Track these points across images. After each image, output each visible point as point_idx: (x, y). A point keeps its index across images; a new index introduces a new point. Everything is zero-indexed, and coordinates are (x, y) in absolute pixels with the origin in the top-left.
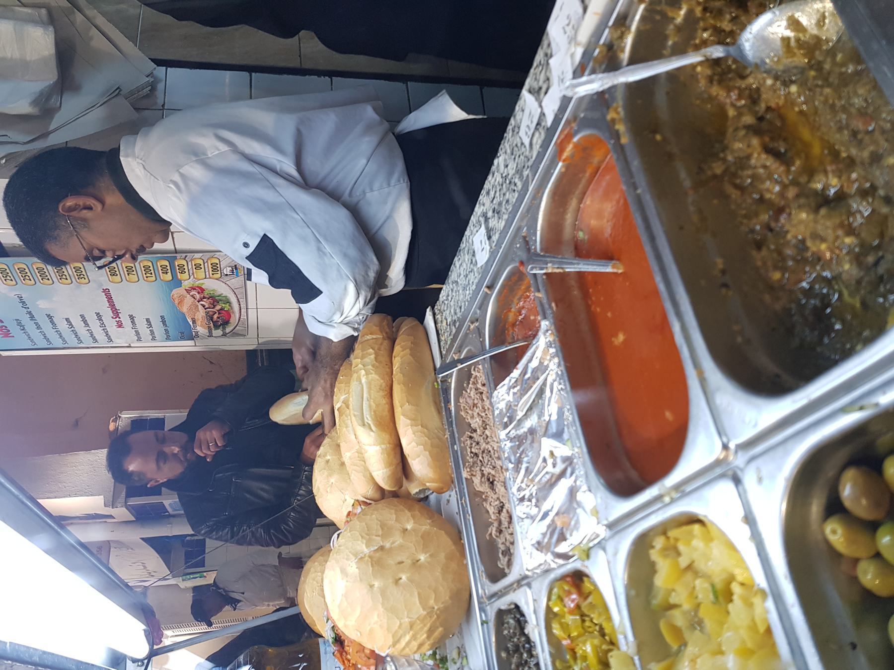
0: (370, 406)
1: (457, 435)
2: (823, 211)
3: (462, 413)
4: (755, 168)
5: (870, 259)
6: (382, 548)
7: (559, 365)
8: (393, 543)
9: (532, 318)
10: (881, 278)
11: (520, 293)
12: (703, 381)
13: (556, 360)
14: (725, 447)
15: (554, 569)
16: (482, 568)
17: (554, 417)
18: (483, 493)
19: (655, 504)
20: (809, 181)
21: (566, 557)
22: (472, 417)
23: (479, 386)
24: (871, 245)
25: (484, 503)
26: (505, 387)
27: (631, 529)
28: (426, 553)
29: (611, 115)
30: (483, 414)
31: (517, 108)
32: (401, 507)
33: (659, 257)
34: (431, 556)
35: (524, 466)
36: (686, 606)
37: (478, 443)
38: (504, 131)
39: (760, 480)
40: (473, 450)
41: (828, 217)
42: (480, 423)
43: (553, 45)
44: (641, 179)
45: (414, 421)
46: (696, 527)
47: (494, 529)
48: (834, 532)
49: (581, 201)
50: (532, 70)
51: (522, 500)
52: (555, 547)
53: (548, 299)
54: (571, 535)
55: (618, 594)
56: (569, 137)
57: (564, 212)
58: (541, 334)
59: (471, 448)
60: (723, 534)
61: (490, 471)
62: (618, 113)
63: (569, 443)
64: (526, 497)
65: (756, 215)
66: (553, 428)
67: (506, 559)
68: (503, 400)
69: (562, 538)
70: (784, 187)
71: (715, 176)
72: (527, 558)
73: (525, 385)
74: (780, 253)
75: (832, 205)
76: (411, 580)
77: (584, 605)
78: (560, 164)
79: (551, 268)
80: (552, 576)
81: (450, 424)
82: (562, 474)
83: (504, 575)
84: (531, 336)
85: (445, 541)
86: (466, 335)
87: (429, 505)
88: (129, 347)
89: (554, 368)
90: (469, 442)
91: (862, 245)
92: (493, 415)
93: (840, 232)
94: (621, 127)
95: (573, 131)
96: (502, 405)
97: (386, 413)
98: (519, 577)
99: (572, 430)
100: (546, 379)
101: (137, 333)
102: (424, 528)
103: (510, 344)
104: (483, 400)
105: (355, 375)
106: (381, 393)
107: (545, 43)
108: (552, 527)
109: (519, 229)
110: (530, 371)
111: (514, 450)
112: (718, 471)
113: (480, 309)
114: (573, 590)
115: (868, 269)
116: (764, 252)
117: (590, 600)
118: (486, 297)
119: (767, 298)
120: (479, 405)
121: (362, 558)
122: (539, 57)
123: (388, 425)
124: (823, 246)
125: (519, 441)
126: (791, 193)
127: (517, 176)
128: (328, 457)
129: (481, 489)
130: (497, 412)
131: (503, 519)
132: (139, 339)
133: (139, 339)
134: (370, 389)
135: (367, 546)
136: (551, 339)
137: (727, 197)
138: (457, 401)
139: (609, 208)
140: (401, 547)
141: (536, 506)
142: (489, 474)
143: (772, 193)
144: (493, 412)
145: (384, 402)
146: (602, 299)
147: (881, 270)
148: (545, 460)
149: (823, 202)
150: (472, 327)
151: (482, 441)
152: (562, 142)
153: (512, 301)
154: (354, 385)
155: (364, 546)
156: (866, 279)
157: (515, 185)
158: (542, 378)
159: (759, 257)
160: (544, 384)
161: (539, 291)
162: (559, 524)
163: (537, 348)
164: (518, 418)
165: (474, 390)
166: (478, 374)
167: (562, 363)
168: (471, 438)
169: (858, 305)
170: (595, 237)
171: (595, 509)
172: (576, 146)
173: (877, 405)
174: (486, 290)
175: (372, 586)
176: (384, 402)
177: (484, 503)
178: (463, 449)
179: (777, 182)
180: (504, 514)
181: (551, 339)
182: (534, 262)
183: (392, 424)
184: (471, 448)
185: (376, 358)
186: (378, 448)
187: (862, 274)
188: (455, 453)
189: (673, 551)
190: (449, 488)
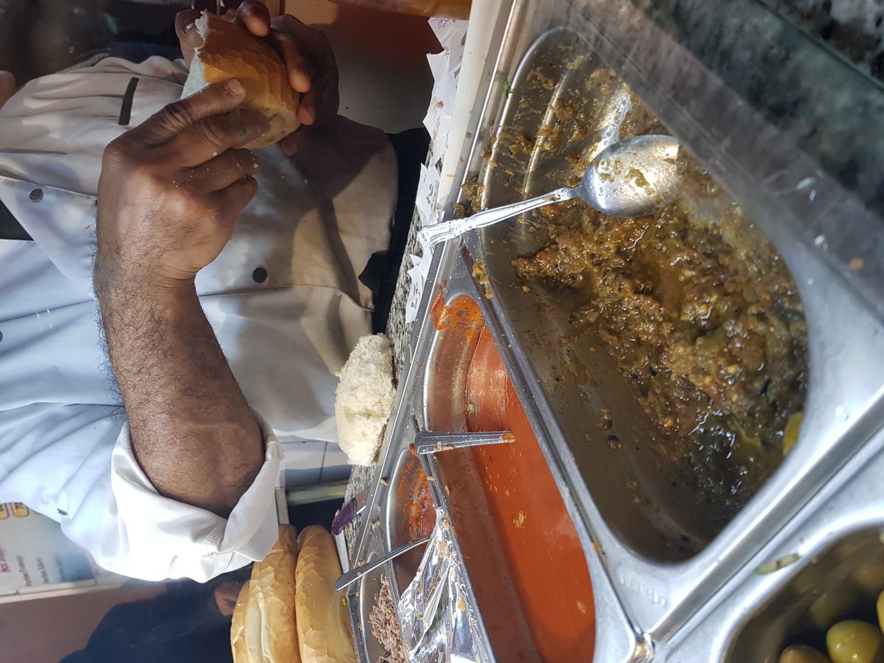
0: (269, 637)
2: (700, 341)
3: (374, 633)
4: (627, 312)
5: (758, 385)
10: (774, 405)
11: (420, 482)
12: (602, 555)
13: (454, 554)
14: (640, 640)
20: (680, 316)
24: (757, 371)
29: (476, 271)
30: (397, 632)
31: (397, 285)
33: (538, 414)
38: (389, 311)
41: (705, 347)
42: (395, 643)
49: (467, 370)
50: (407, 246)
53: (440, 482)
56: (442, 301)
62: (480, 268)
71: (589, 324)
74: (667, 397)
78: (437, 332)
79: (440, 447)
86: (370, 537)
88: (17, 594)
93: (721, 361)
96: (408, 618)
97: (288, 643)
101: (26, 576)
103: (414, 542)
105: (252, 600)
107: (415, 217)
115: (757, 397)
116: (651, 398)
118: (385, 490)
119: (663, 449)
120: (392, 621)
124: (708, 380)
126: (666, 330)
132: (29, 584)
133: (29, 584)
134: (269, 615)
137: (605, 344)
138: (367, 619)
145: (286, 629)
147: (772, 395)
150: (373, 527)
152: (435, 309)
156: (758, 409)
159: (648, 404)
161: (431, 475)
164: (425, 631)
165: (384, 603)
167: (460, 556)
169: (759, 444)
170: (487, 410)
174: (383, 482)
176: (286, 629)
179: (651, 322)
183: (296, 657)
185: (276, 577)
187: (752, 403)
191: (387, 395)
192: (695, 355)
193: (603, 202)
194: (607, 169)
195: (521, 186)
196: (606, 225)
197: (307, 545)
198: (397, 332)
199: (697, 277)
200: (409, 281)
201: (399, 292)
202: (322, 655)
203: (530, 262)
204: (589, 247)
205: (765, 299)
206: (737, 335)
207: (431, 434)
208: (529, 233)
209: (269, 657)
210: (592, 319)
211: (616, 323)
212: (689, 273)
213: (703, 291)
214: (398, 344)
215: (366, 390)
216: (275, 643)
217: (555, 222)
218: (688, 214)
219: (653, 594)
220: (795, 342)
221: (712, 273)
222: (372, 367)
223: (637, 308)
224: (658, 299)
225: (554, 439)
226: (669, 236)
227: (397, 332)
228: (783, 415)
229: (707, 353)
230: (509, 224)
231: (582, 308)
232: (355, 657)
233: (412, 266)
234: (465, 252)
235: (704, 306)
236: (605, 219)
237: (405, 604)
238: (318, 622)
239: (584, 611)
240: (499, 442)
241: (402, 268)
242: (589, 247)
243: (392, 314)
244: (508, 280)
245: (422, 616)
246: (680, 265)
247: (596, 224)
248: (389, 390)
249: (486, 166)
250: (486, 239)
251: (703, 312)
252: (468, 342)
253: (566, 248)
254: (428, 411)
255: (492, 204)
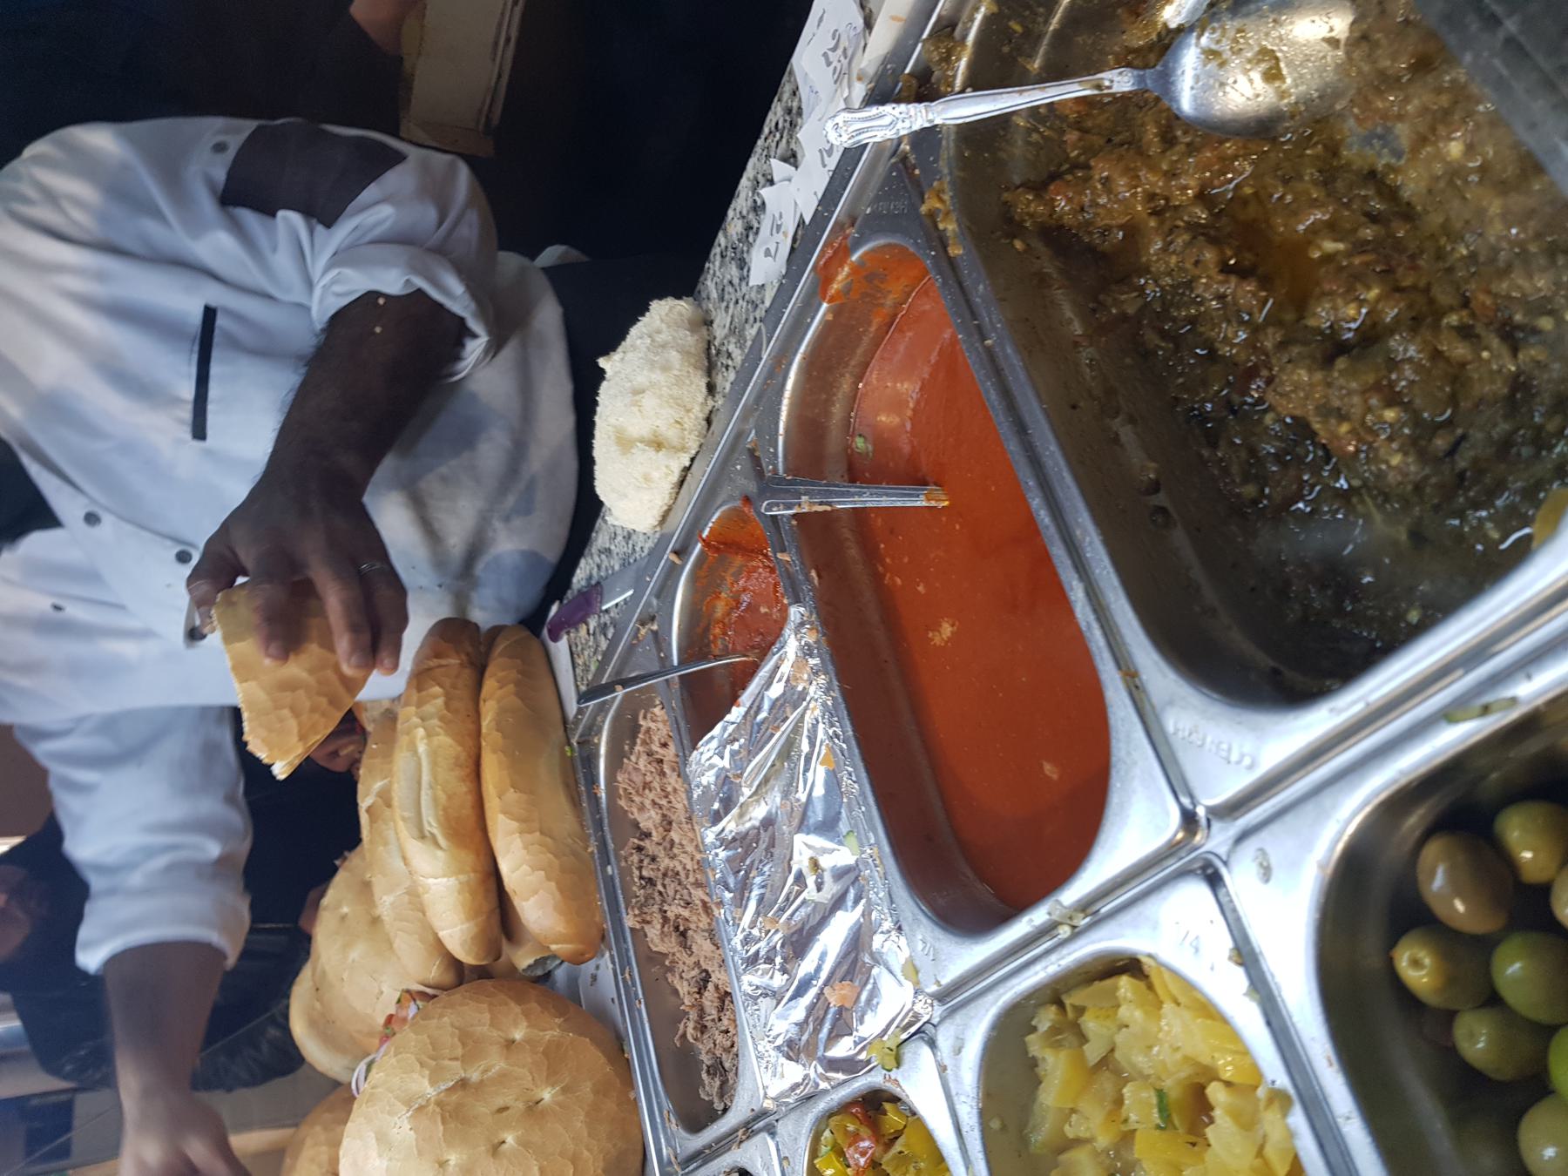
0: (435, 800)
1: (611, 846)
2: (1341, 363)
3: (622, 803)
5: (1441, 443)
6: (463, 1084)
7: (827, 691)
8: (486, 1071)
9: (763, 610)
10: (1461, 476)
13: (822, 679)
15: (825, 1091)
16: (667, 1105)
17: (819, 791)
18: (665, 955)
19: (1032, 949)
20: (1301, 318)
21: (850, 1066)
22: (642, 808)
23: (655, 747)
25: (669, 975)
26: (714, 744)
27: (990, 997)
28: (553, 1086)
30: (664, 802)
31: (730, 213)
32: (502, 996)
33: (1036, 462)
34: (564, 1090)
35: (756, 893)
36: (1103, 1141)
37: (654, 859)
38: (705, 256)
39: (1266, 873)
40: (645, 873)
41: (1348, 373)
42: (658, 818)
43: (804, 92)
44: (994, 319)
45: (526, 822)
46: (1125, 983)
47: (691, 1025)
48: (1416, 963)
50: (760, 142)
51: (752, 961)
52: (826, 1049)
54: (861, 1021)
55: (965, 1129)
57: (829, 402)
58: (788, 632)
59: (640, 868)
60: (1189, 986)
61: (681, 911)
62: (941, 200)
63: (852, 840)
64: (762, 953)
65: (1205, 383)
66: (817, 814)
67: (718, 1083)
68: (712, 767)
69: (842, 1027)
70: (1255, 330)
71: (1124, 317)
72: (767, 1077)
73: (756, 733)
74: (1253, 451)
75: (1355, 352)
76: (524, 1144)
77: (887, 1159)
78: (825, 305)
79: (806, 505)
80: (822, 1106)
81: (599, 825)
82: (838, 903)
83: (713, 1116)
84: (765, 641)
85: (592, 1057)
86: (631, 649)
87: (553, 987)
89: (819, 694)
90: (635, 858)
91: (1417, 421)
92: (690, 798)
94: (950, 227)
95: (849, 242)
96: (709, 778)
97: (468, 811)
98: (747, 1114)
99: (859, 812)
100: (803, 716)
102: (548, 1035)
103: (716, 658)
104: (662, 774)
105: (403, 740)
106: (458, 772)
107: (786, 89)
108: (816, 1012)
109: (739, 436)
110: (766, 706)
111: (734, 864)
112: (1173, 866)
113: (658, 596)
114: (865, 1131)
117: (898, 1147)
118: (672, 572)
120: (656, 785)
121: (421, 1108)
122: (776, 114)
123: (472, 834)
124: (1344, 428)
125: (743, 843)
127: (733, 340)
128: (345, 910)
129: (662, 948)
130: (697, 793)
131: (707, 1003)
134: (434, 764)
135: (433, 1082)
136: (810, 638)
139: (909, 389)
140: (503, 1078)
141: (784, 971)
142: (678, 916)
143: (1233, 345)
144: (689, 792)
145: (463, 789)
146: (906, 560)
148: (800, 878)
149: (1332, 349)
150: (643, 631)
151: (662, 854)
153: (723, 579)
154: (401, 760)
155: (426, 1082)
156: (1433, 480)
157: (729, 356)
158: (793, 717)
160: (797, 729)
161: (783, 550)
162: (834, 1000)
163: (781, 659)
165: (644, 757)
166: (653, 725)
168: (640, 849)
169: (1403, 536)
171: (914, 961)
172: (856, 270)
173: (1514, 701)
174: (674, 558)
175: (442, 1164)
176: (464, 789)
177: (669, 975)
178: (625, 873)
179: (1242, 323)
180: (710, 995)
181: (810, 638)
182: (774, 494)
184: (640, 868)
185: (447, 705)
186: (452, 881)
187: (1427, 471)
188: (609, 882)
189: (1071, 1031)
190: (597, 953)
191: (697, 408)
192: (1329, 385)
193: (1186, 103)
194: (1218, 42)
195: (1030, 56)
196: (1188, 145)
197: (501, 655)
198: (722, 299)
199: (1349, 254)
200: (758, 208)
201: (734, 226)
202: (530, 832)
203: (1038, 196)
204: (1152, 181)
205: (1483, 304)
206: (1410, 360)
207: (790, 483)
208: (1029, 143)
209: (436, 831)
210: (1131, 310)
211: (1174, 320)
212: (1330, 246)
213: (1355, 279)
214: (721, 323)
215: (660, 397)
216: (445, 809)
217: (1078, 125)
218: (1342, 140)
219: (1229, 750)
220: (1522, 379)
221: (1374, 250)
222: (674, 356)
223: (1221, 297)
224: (1266, 282)
225: (1066, 504)
226: (1300, 178)
227: (722, 299)
228: (1471, 494)
229: (1354, 385)
230: (1001, 123)
231: (1114, 287)
232: (585, 839)
233: (771, 182)
234: (909, 164)
235: (1353, 305)
236: (1185, 133)
237: (704, 757)
238: (521, 779)
239: (1055, 777)
240: (918, 504)
241: (744, 182)
242: (1152, 181)
243: (714, 265)
244: (993, 226)
245: (740, 776)
246: (1314, 230)
247: (1168, 140)
248: (701, 399)
249: (977, 9)
250: (957, 147)
251: (1352, 316)
252: (873, 329)
253: (1107, 178)
254: (785, 443)
255: (980, 81)
